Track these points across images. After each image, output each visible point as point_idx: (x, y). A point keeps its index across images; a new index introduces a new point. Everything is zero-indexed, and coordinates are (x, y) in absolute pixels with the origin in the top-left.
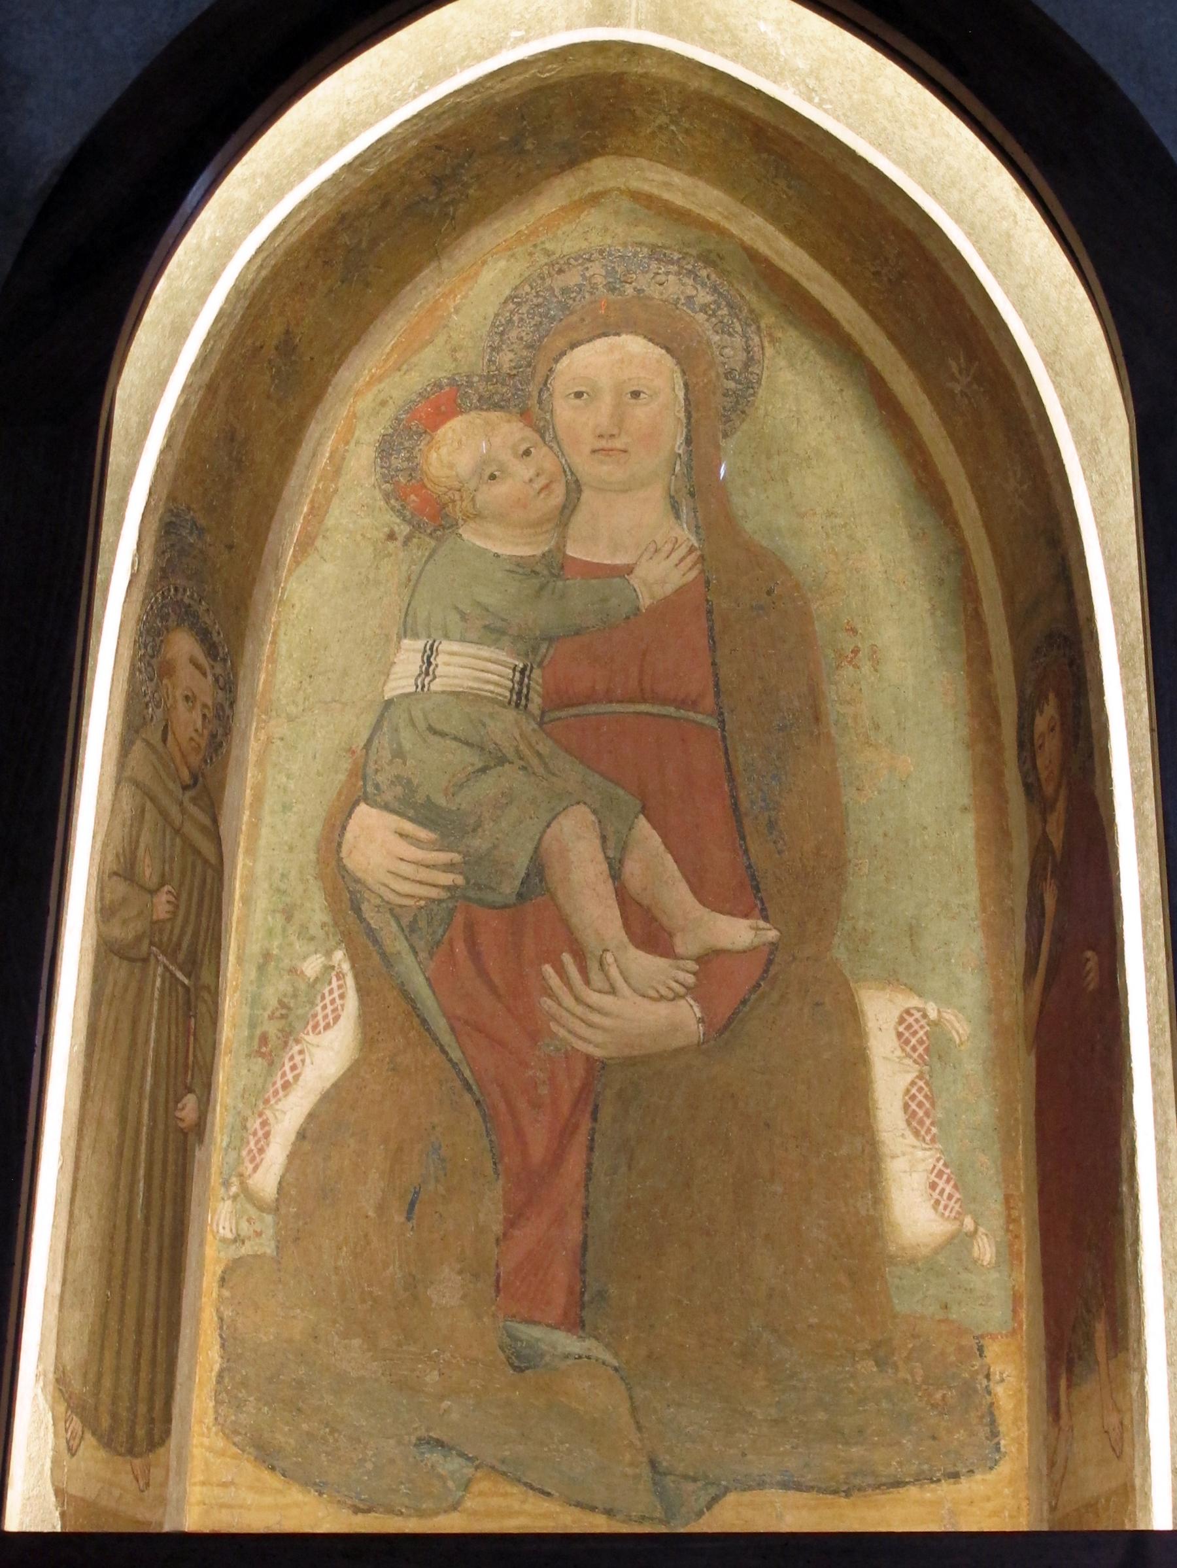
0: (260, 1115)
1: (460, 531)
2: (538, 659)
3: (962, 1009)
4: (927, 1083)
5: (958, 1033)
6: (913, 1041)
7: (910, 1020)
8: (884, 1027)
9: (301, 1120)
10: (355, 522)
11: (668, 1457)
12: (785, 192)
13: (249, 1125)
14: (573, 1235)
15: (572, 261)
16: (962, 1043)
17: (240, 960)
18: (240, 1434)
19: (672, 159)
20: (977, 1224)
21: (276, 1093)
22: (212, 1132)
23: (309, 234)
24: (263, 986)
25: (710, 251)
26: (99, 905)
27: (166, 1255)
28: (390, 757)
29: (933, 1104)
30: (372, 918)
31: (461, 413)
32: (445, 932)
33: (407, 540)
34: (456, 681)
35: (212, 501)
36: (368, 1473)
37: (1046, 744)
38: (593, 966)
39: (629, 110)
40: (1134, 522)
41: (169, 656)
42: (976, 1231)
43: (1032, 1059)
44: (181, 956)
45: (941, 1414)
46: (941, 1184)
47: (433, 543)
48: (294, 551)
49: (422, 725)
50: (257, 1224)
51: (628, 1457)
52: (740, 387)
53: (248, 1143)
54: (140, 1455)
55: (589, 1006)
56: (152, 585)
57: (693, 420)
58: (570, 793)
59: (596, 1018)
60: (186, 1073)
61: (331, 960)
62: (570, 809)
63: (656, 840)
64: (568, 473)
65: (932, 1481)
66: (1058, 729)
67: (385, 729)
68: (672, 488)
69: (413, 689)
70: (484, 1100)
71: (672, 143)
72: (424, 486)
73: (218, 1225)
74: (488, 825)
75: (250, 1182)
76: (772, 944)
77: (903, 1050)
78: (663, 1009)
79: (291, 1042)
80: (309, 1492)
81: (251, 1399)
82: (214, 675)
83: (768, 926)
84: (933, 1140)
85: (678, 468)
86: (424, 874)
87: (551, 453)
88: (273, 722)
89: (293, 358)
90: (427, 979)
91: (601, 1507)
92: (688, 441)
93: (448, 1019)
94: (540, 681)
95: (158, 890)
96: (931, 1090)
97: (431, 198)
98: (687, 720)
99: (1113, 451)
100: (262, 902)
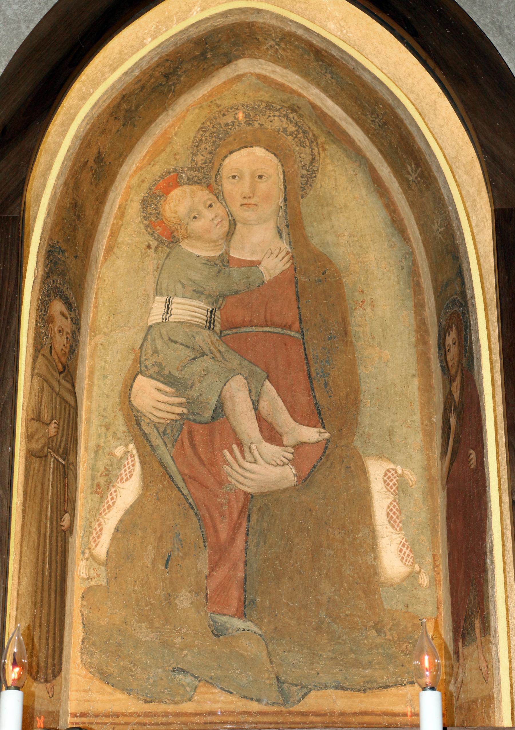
0: (98, 521)
1: (181, 244)
2: (218, 306)
3: (413, 469)
4: (397, 503)
5: (411, 480)
6: (391, 484)
7: (390, 474)
8: (378, 478)
9: (116, 523)
10: (132, 240)
11: (284, 675)
12: (330, 80)
13: (92, 525)
14: (241, 575)
15: (229, 110)
16: (413, 485)
17: (86, 449)
18: (92, 667)
19: (276, 60)
20: (420, 568)
21: (105, 510)
22: (76, 529)
23: (108, 106)
24: (97, 461)
25: (294, 105)
26: (26, 435)
27: (58, 589)
28: (151, 353)
29: (400, 513)
30: (146, 428)
31: (179, 186)
32: (179, 435)
33: (157, 248)
34: (181, 317)
35: (68, 237)
36: (151, 685)
37: (451, 349)
38: (247, 450)
39: (256, 38)
40: (492, 241)
41: (51, 313)
42: (420, 571)
43: (445, 493)
44: (61, 451)
45: (405, 655)
46: (404, 550)
47: (168, 250)
48: (104, 254)
49: (166, 338)
50: (98, 571)
51: (267, 675)
52: (309, 173)
53: (93, 534)
54: (50, 682)
55: (245, 469)
56: (43, 282)
57: (287, 190)
58: (235, 370)
59: (248, 474)
60: (64, 505)
61: (127, 449)
62: (235, 377)
63: (274, 391)
64: (230, 216)
65: (402, 685)
66: (457, 344)
67: (149, 340)
68: (278, 223)
69: (161, 320)
70: (199, 513)
71: (276, 54)
72: (163, 222)
73: (80, 572)
74: (197, 385)
75: (94, 551)
76: (327, 439)
77: (386, 488)
78: (279, 470)
79: (111, 487)
80: (124, 694)
81: (97, 651)
82: (71, 318)
83: (325, 431)
84: (400, 530)
85: (280, 213)
86: (169, 408)
87: (222, 207)
88: (97, 337)
89: (102, 164)
90: (172, 457)
91: (255, 698)
92: (285, 200)
93: (182, 475)
94: (220, 316)
95: (50, 423)
96: (399, 507)
97: (163, 83)
98: (287, 335)
99: (483, 207)
100: (95, 421)
